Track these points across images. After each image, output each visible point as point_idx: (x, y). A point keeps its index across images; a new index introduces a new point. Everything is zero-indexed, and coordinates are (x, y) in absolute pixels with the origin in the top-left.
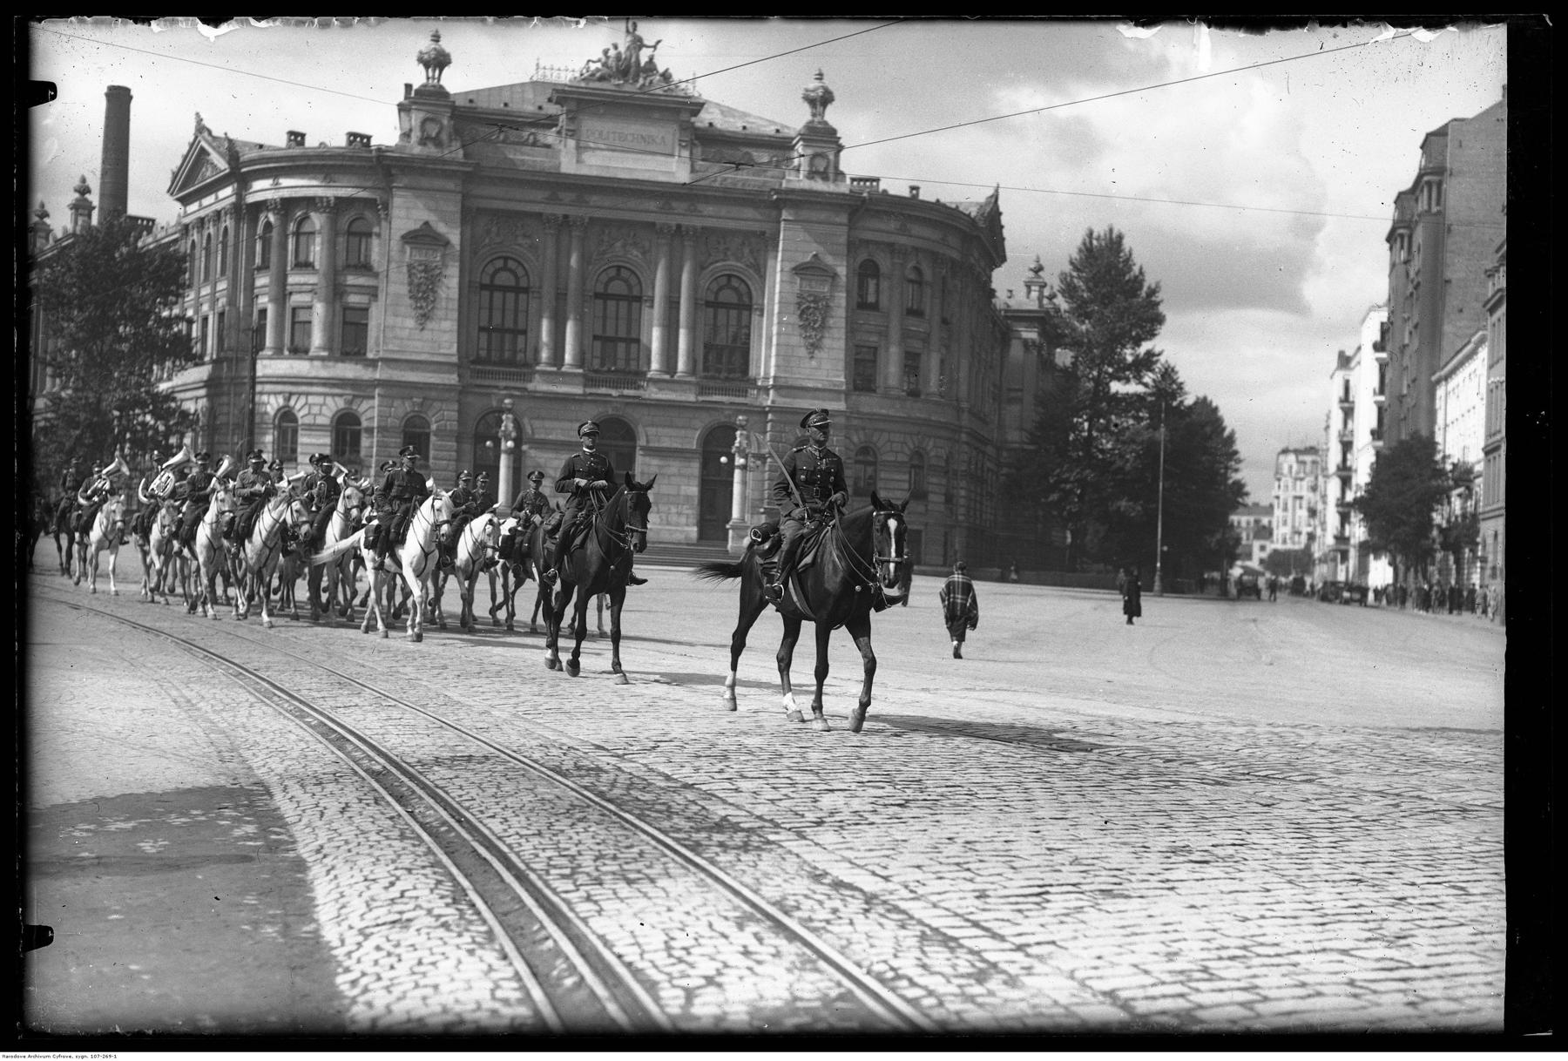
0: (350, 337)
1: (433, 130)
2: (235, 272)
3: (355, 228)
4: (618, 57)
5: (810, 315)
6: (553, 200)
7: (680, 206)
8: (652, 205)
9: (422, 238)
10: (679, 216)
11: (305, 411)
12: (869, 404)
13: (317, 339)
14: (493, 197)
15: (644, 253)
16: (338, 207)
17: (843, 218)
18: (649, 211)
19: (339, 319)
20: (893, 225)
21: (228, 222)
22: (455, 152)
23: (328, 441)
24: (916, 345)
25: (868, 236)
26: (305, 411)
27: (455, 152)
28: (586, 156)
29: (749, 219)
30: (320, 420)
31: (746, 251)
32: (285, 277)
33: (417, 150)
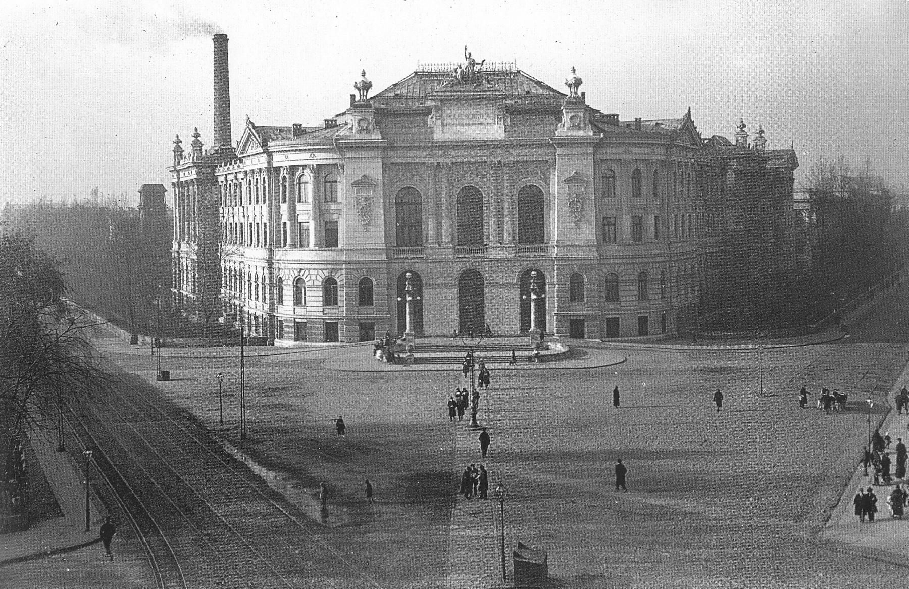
0: (329, 237)
1: (364, 125)
2: (270, 199)
3: (328, 179)
4: (462, 72)
5: (576, 205)
6: (432, 155)
7: (500, 152)
8: (485, 152)
9: (362, 183)
10: (501, 156)
11: (308, 278)
12: (612, 249)
13: (312, 240)
14: (396, 157)
15: (482, 178)
16: (318, 170)
17: (591, 150)
18: (483, 155)
19: (323, 228)
20: (619, 150)
21: (264, 175)
22: (376, 137)
23: (321, 293)
24: (639, 212)
25: (604, 157)
26: (308, 278)
27: (376, 137)
28: (446, 129)
29: (536, 154)
30: (316, 283)
31: (539, 171)
32: (295, 206)
33: (358, 137)
